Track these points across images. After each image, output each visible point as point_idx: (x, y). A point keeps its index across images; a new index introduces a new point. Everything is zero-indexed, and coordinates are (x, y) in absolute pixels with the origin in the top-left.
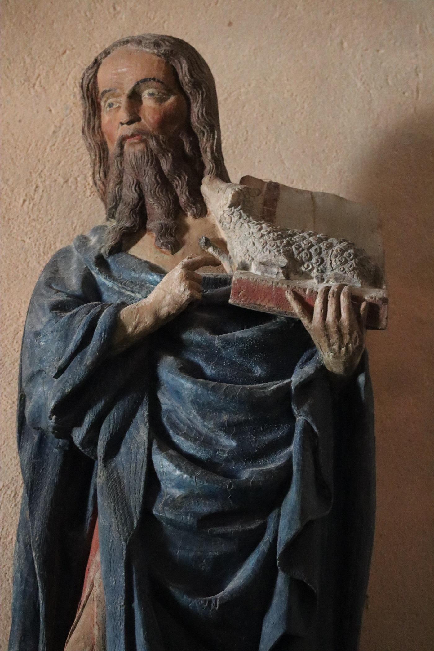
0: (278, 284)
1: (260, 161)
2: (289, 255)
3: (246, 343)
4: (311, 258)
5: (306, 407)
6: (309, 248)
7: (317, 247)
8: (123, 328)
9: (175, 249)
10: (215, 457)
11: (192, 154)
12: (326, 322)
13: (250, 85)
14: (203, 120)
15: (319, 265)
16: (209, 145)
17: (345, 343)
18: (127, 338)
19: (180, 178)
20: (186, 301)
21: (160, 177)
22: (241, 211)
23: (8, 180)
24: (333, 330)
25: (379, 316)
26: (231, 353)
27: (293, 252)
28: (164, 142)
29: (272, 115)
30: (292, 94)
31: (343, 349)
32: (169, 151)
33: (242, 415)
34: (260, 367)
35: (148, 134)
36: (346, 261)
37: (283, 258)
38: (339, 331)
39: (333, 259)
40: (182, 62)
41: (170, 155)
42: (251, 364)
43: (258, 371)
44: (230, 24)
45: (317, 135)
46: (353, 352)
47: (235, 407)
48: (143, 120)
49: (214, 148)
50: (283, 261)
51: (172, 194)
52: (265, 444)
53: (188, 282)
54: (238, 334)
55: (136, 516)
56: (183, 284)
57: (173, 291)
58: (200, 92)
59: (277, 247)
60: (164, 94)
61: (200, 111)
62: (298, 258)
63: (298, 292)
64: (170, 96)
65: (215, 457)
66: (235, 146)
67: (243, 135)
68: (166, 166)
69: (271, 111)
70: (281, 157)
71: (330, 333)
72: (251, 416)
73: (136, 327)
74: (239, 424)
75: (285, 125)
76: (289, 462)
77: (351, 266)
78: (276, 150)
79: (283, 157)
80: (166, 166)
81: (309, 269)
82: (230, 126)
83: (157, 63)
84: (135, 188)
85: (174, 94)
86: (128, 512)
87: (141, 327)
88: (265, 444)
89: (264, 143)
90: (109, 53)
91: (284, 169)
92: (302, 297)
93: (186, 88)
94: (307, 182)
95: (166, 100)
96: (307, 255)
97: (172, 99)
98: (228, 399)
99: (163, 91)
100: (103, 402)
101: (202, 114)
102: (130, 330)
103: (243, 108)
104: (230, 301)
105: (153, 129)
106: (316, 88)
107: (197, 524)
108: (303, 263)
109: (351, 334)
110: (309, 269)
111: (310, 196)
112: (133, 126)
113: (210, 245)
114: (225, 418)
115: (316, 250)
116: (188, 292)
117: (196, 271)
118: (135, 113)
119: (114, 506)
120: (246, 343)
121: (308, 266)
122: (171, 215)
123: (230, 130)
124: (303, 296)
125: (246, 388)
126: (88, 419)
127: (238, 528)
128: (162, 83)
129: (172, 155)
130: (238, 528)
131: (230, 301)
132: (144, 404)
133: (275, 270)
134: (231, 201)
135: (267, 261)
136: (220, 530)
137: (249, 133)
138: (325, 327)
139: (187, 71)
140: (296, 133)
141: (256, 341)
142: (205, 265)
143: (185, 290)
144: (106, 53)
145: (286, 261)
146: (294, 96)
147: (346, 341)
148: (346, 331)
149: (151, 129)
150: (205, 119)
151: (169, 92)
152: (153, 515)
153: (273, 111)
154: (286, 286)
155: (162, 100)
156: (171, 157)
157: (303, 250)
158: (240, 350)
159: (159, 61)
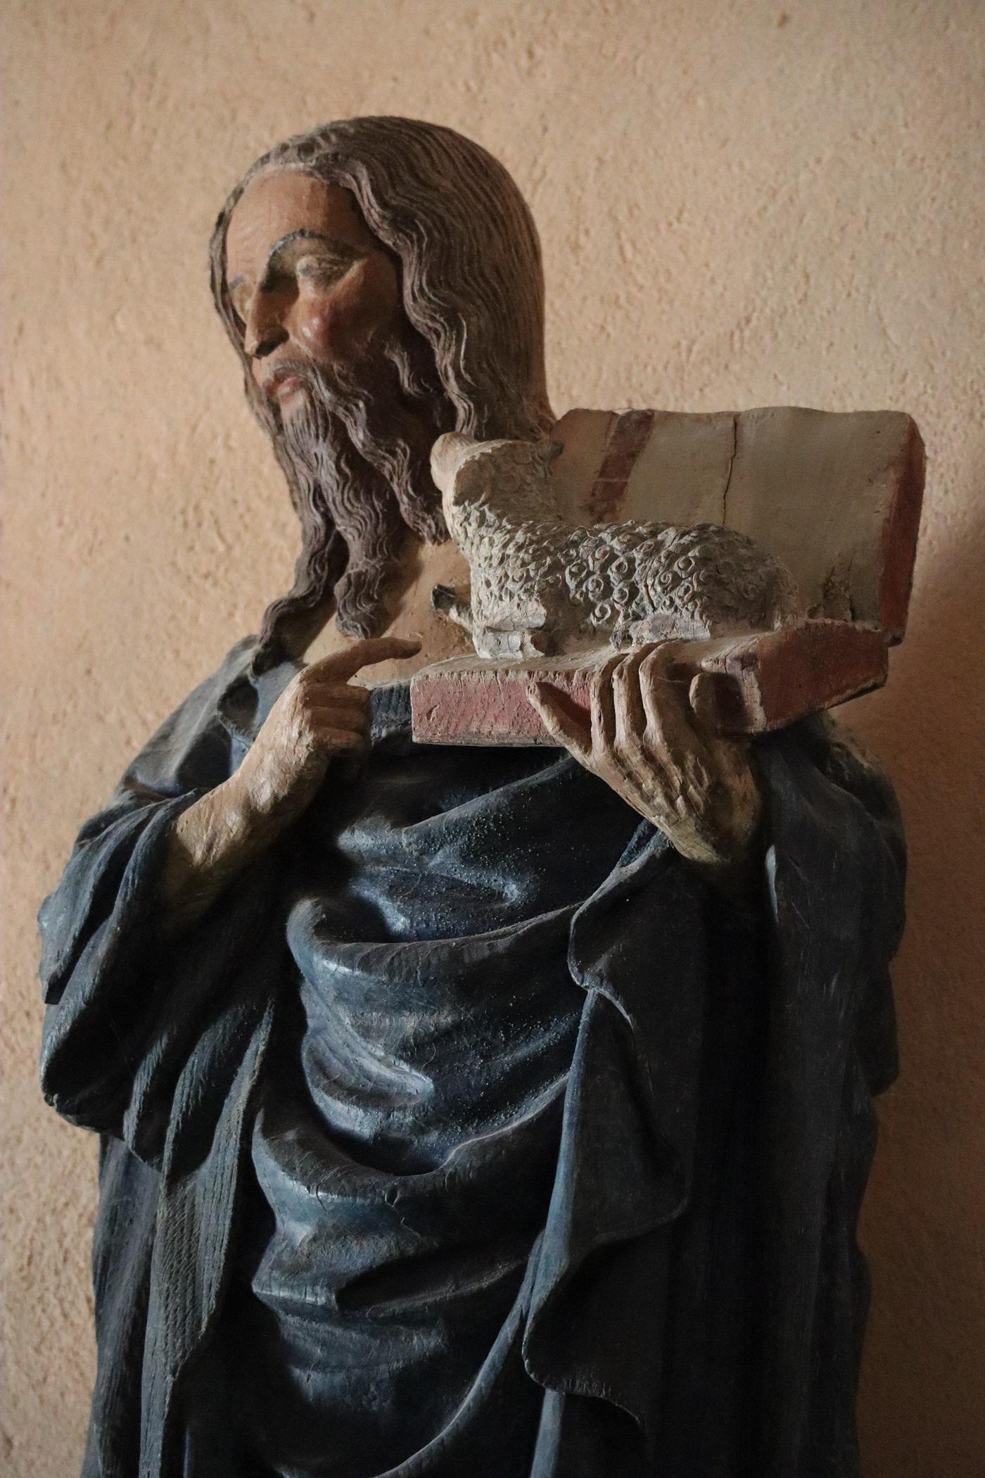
0: (507, 672)
1: (832, 344)
2: (555, 596)
3: (473, 830)
4: (608, 591)
5: (601, 964)
6: (604, 568)
7: (622, 559)
8: (184, 853)
9: (373, 632)
10: (389, 1127)
11: (417, 389)
12: (616, 743)
13: (819, 161)
14: (423, 302)
15: (628, 604)
16: (449, 358)
17: (677, 784)
18: (197, 877)
19: (394, 454)
20: (308, 759)
21: (348, 463)
22: (486, 508)
23: (284, 526)
24: (635, 759)
25: (743, 702)
26: (442, 860)
27: (565, 585)
28: (345, 379)
29: (867, 223)
30: (914, 159)
31: (680, 801)
32: (358, 396)
33: (446, 1012)
34: (517, 880)
35: (305, 363)
36: (677, 580)
37: (536, 605)
38: (649, 757)
39: (649, 582)
40: (359, 175)
41: (361, 405)
42: (494, 880)
43: (513, 891)
44: (784, 20)
45: (966, 244)
46: (706, 803)
47: (421, 997)
48: (292, 337)
49: (462, 363)
50: (536, 613)
51: (380, 496)
52: (503, 1073)
53: (308, 713)
54: (454, 814)
55: (208, 1303)
56: (297, 721)
57: (277, 743)
58: (415, 236)
59: (528, 578)
60: (332, 262)
61: (417, 282)
62: (578, 596)
63: (555, 684)
64: (350, 265)
65: (389, 1127)
66: (778, 320)
67: (796, 289)
68: (358, 436)
69: (863, 212)
70: (881, 319)
71: (634, 769)
72: (468, 1010)
73: (210, 847)
74: (444, 1036)
75: (893, 239)
76: (555, 1109)
77: (687, 591)
78: (871, 308)
79: (886, 321)
80: (358, 436)
81: (607, 616)
82: (769, 274)
83: (308, 191)
84: (314, 500)
85: (359, 256)
86: (193, 1301)
87: (222, 842)
88: (503, 1073)
89: (844, 296)
90: (241, 192)
91: (887, 350)
92: (565, 694)
93: (382, 234)
94: (937, 371)
95: (340, 275)
96: (598, 585)
97: (354, 270)
98: (396, 980)
99: (330, 256)
100: (165, 1040)
101: (421, 289)
102: (198, 855)
103: (801, 221)
104: (415, 739)
105: (315, 352)
106: (970, 127)
107: (338, 1299)
108: (591, 607)
109: (679, 760)
110: (607, 616)
111: (731, 424)
112: (278, 353)
113: (451, 602)
114: (409, 1023)
115: (619, 567)
116: (308, 738)
117: (353, 682)
118: (273, 325)
119: (168, 1290)
120: (473, 830)
121: (603, 611)
122: (381, 549)
123: (770, 282)
124: (566, 689)
125: (449, 945)
126: (140, 1085)
127: (446, 1292)
128: (321, 237)
129: (366, 404)
130: (446, 1292)
131: (415, 739)
132: (264, 1026)
133: (516, 639)
134: (456, 489)
135: (502, 621)
136: (397, 1306)
137: (812, 281)
138: (618, 759)
139: (370, 194)
140: (918, 252)
141: (496, 820)
142: (395, 656)
143: (300, 734)
144: (238, 194)
145: (543, 611)
146: (918, 162)
147: (677, 781)
148: (664, 756)
149: (310, 354)
150: (429, 300)
151: (344, 253)
152: (253, 1297)
153: (868, 211)
154: (526, 675)
155: (330, 277)
156: (363, 411)
157: (590, 574)
158: (462, 850)
159: (313, 186)
